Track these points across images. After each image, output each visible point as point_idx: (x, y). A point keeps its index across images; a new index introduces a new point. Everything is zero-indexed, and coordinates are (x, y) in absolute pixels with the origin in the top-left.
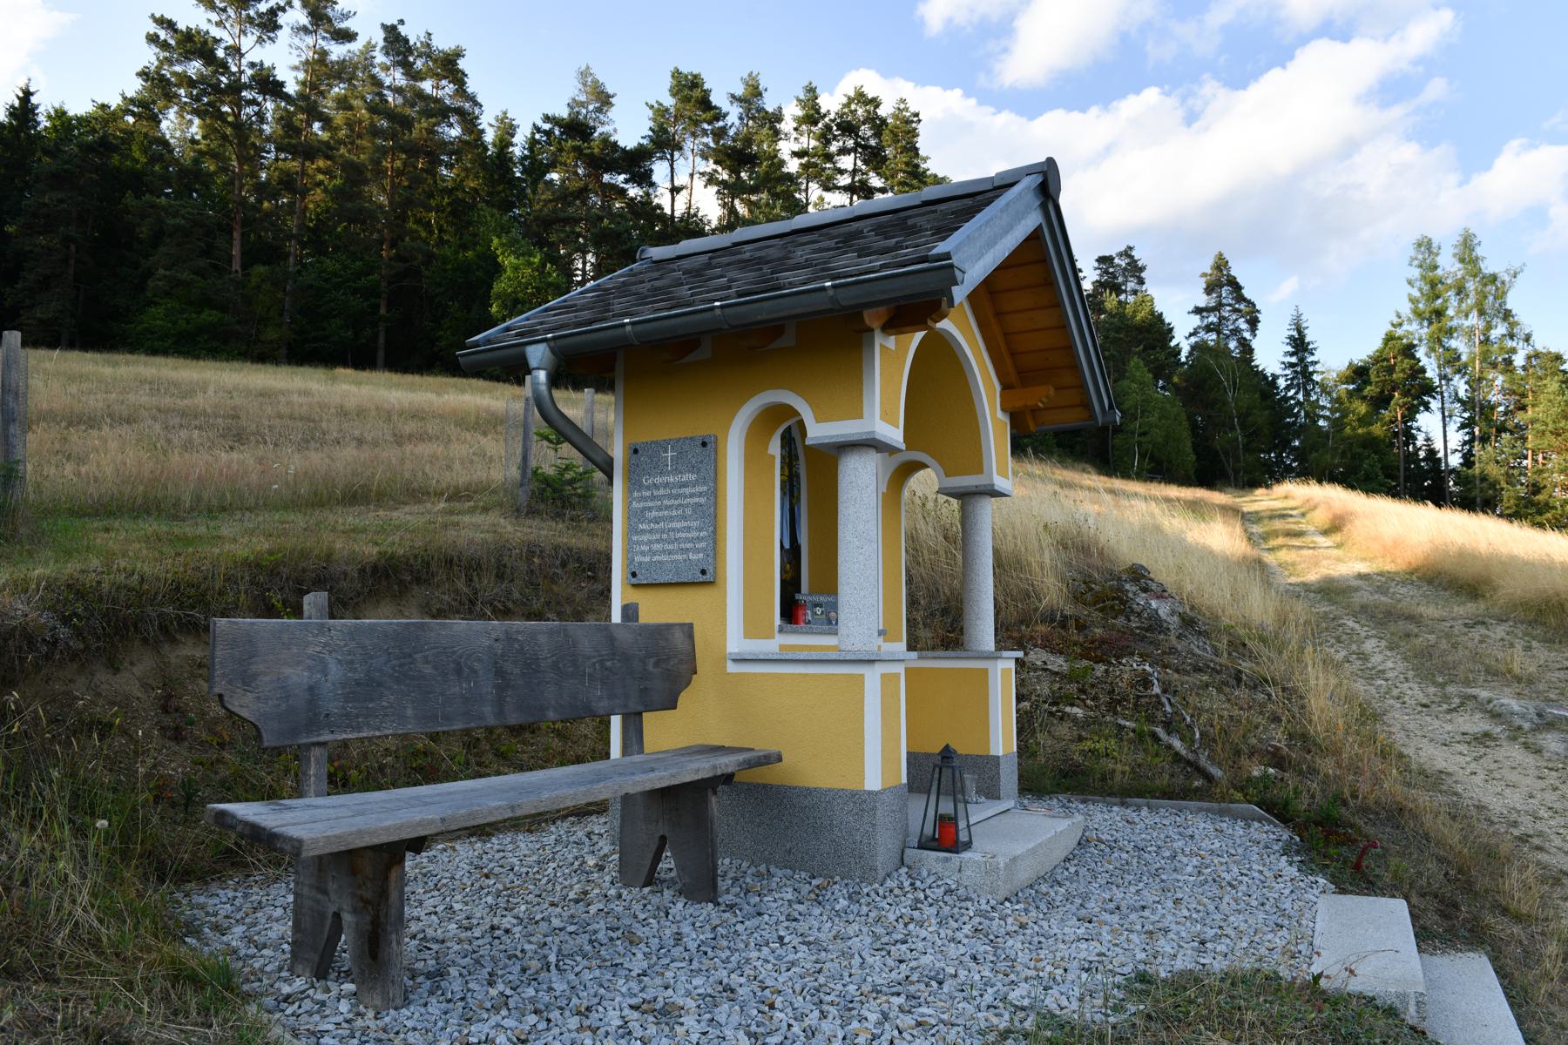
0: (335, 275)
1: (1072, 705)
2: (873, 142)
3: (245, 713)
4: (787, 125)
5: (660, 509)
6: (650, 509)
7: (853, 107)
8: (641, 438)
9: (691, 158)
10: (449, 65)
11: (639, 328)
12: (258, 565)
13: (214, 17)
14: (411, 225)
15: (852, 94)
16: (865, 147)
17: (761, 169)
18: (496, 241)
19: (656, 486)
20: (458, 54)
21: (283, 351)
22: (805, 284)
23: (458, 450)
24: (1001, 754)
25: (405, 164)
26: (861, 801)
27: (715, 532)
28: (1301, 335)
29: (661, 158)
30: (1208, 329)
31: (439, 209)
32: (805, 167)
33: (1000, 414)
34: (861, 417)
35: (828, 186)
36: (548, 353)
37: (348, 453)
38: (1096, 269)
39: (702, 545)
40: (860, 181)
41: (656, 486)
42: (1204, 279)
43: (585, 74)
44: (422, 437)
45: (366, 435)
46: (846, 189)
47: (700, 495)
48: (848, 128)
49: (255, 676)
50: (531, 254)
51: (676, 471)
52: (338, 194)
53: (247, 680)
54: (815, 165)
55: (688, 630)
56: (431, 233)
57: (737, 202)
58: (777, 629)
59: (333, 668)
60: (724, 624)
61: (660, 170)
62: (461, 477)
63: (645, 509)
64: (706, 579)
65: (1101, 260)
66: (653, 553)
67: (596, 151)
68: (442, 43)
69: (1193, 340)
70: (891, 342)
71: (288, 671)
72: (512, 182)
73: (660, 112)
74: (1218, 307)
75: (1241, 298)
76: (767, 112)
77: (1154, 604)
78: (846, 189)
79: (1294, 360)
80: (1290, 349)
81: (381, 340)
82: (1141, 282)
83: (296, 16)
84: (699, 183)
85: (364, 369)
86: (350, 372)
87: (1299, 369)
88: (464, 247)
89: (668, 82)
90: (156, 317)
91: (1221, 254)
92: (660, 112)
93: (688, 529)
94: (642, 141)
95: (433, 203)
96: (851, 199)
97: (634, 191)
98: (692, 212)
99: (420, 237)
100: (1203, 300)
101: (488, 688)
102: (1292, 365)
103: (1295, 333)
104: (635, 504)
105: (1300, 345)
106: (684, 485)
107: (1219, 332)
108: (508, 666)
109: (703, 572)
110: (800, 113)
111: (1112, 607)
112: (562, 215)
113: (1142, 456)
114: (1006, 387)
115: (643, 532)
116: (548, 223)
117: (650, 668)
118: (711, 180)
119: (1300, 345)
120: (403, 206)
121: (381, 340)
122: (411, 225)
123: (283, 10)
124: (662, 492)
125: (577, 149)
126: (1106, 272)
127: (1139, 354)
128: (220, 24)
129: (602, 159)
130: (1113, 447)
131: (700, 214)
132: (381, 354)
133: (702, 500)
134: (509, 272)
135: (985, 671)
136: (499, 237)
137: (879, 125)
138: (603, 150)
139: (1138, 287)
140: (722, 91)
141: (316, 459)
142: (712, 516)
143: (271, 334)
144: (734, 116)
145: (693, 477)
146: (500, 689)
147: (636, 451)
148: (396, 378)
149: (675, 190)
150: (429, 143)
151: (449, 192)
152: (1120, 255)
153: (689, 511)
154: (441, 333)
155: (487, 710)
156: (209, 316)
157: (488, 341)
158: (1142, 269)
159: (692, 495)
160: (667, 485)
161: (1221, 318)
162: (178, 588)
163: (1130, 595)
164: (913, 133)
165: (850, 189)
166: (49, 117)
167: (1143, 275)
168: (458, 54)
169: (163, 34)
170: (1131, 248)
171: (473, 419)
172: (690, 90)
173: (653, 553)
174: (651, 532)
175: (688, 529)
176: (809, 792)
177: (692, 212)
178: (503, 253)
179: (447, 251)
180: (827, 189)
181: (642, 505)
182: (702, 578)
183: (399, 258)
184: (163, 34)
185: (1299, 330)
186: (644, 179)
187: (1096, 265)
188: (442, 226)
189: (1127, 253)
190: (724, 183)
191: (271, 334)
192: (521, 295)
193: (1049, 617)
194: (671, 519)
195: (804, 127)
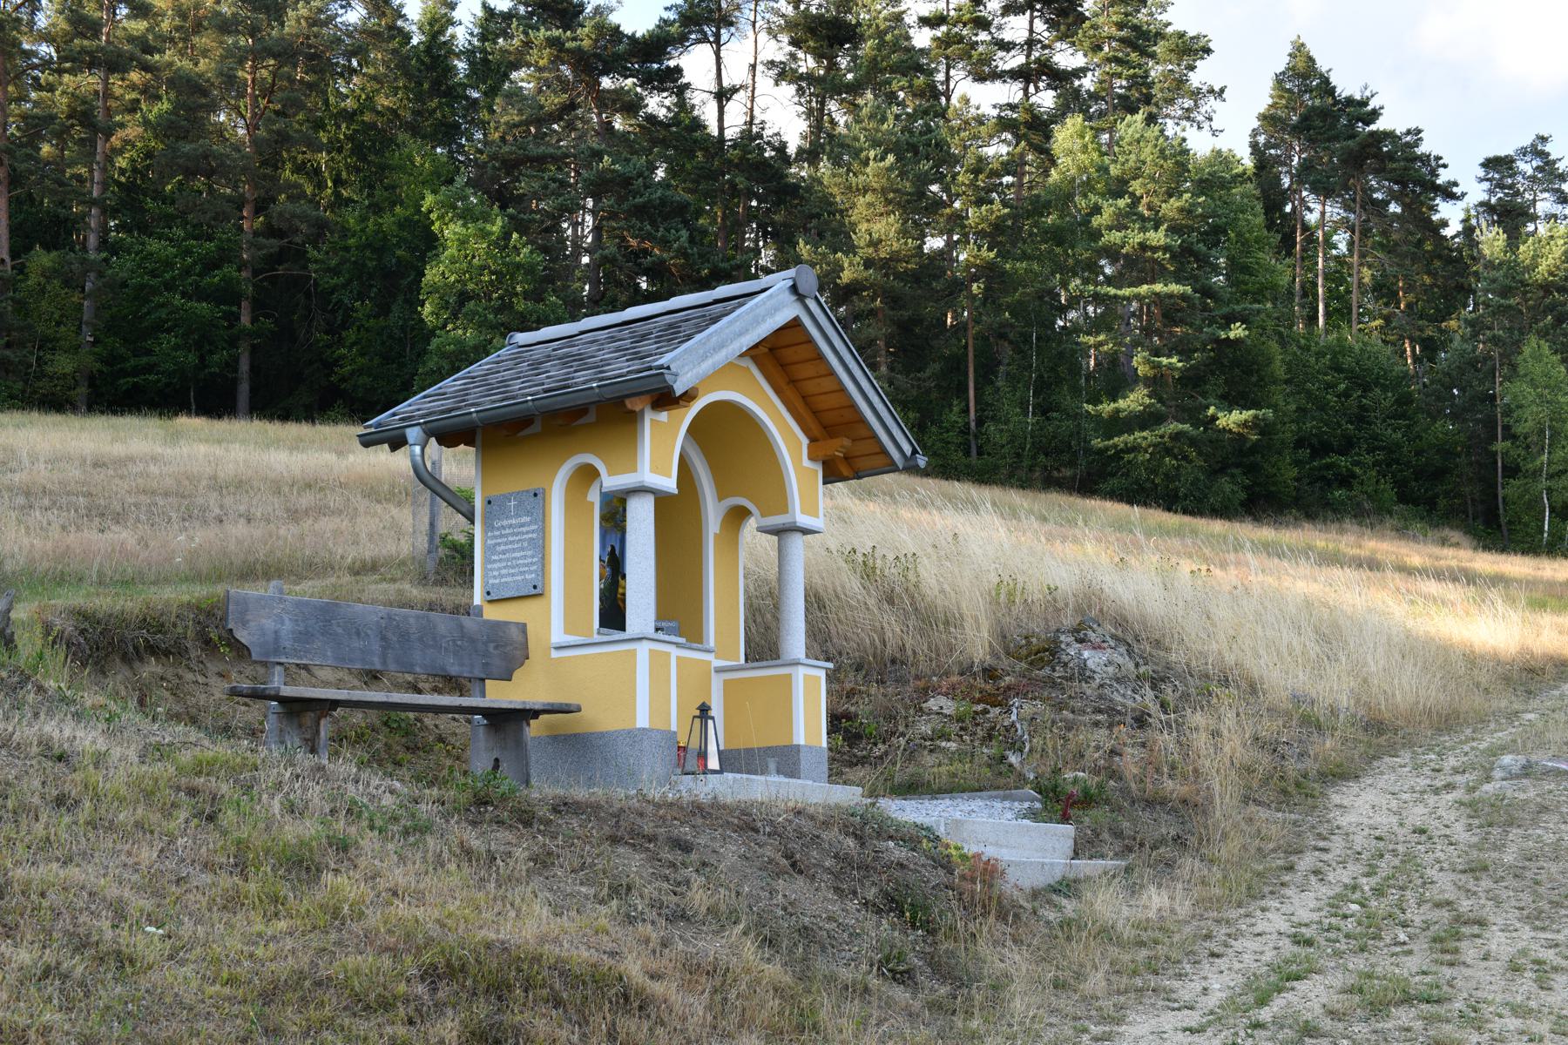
0: (169, 264)
1: (949, 740)
3: (243, 641)
5: (506, 544)
6: (499, 544)
8: (494, 493)
9: (751, 34)
11: (482, 414)
12: (198, 608)
14: (287, 174)
17: (867, 47)
18: (429, 200)
19: (503, 527)
21: (83, 390)
22: (584, 384)
23: (365, 525)
24: (802, 742)
25: (274, 74)
26: (636, 736)
27: (543, 558)
29: (698, 41)
31: (334, 147)
32: (944, 43)
33: (806, 463)
34: (635, 471)
35: (984, 73)
36: (421, 433)
37: (239, 530)
38: (1481, 180)
39: (535, 567)
40: (1038, 61)
41: (503, 527)
44: (322, 511)
45: (253, 510)
46: (1015, 74)
47: (533, 531)
49: (248, 621)
50: (486, 218)
51: (517, 516)
52: (167, 129)
53: (244, 623)
54: (960, 39)
55: (523, 628)
56: (321, 186)
57: (832, 106)
58: (595, 631)
59: (287, 622)
60: (549, 624)
61: (695, 64)
62: (368, 551)
63: (496, 544)
64: (536, 593)
65: (1491, 164)
66: (502, 576)
67: (586, 43)
70: (663, 416)
71: (264, 621)
72: (452, 94)
77: (1086, 654)
78: (1015, 74)
81: (244, 366)
84: (765, 82)
85: (220, 417)
86: (198, 422)
88: (376, 209)
93: (525, 557)
94: (666, 15)
95: (323, 137)
96: (1026, 90)
97: (657, 104)
98: (755, 129)
99: (303, 195)
101: (376, 646)
104: (489, 542)
106: (522, 525)
108: (389, 635)
109: (535, 587)
111: (1042, 659)
112: (535, 150)
114: (813, 440)
115: (495, 561)
116: (511, 166)
117: (491, 650)
118: (784, 73)
120: (271, 151)
121: (244, 366)
122: (287, 174)
124: (507, 531)
125: (553, 42)
126: (1501, 186)
127: (1543, 334)
129: (595, 55)
130: (1504, 498)
131: (767, 133)
132: (244, 389)
133: (534, 535)
134: (451, 251)
135: (790, 675)
136: (434, 192)
138: (596, 41)
141: (201, 537)
142: (541, 547)
143: (63, 364)
145: (528, 519)
146: (384, 648)
147: (489, 502)
148: (274, 429)
149: (723, 95)
150: (312, 41)
151: (349, 116)
152: (1523, 152)
153: (525, 544)
154: (343, 351)
155: (376, 660)
157: (379, 425)
159: (527, 532)
160: (510, 526)
162: (145, 620)
163: (1063, 646)
165: (1023, 75)
170: (1544, 139)
171: (386, 487)
173: (502, 576)
174: (500, 561)
175: (525, 557)
176: (602, 735)
177: (755, 129)
178: (441, 217)
179: (351, 219)
180: (980, 78)
181: (493, 542)
182: (534, 592)
183: (270, 231)
186: (670, 80)
187: (1481, 173)
188: (339, 175)
189: (1537, 150)
190: (810, 77)
191: (63, 364)
192: (471, 286)
194: (514, 550)
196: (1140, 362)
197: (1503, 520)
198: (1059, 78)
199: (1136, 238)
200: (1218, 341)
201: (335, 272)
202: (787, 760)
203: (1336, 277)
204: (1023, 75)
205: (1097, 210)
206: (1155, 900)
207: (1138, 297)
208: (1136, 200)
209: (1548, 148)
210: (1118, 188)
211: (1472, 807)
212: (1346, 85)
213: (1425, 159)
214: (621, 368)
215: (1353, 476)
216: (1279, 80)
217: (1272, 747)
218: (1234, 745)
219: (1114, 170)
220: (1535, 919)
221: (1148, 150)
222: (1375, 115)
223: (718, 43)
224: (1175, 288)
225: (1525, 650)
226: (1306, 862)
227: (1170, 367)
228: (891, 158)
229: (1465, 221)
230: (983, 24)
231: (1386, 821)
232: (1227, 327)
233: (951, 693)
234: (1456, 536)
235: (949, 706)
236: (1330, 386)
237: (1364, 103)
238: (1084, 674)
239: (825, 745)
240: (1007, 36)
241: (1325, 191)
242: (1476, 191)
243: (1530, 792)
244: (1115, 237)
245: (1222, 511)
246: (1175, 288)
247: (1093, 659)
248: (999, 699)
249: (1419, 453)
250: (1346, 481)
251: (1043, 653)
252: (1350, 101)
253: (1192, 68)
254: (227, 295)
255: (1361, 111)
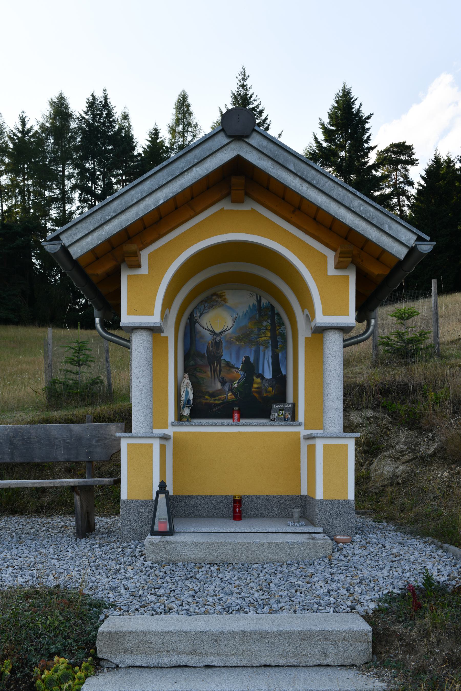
239: (351, 496)
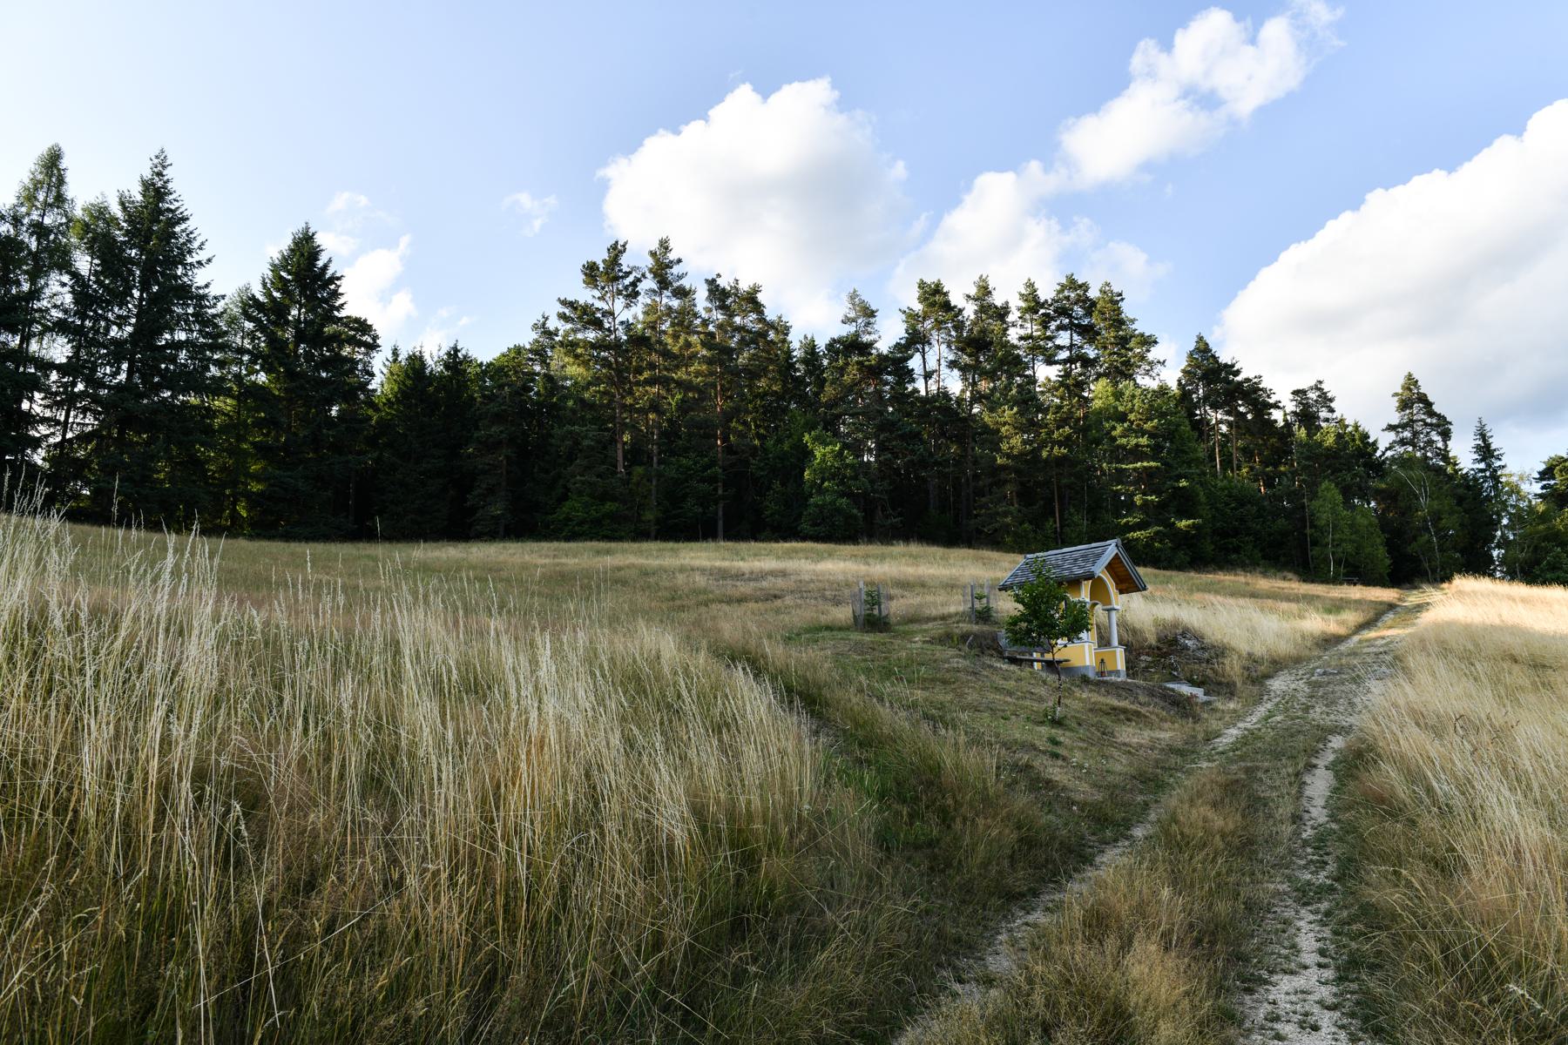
2: (1085, 322)
4: (1013, 317)
7: (1066, 293)
10: (751, 301)
13: (597, 293)
15: (1064, 281)
16: (1079, 326)
18: (806, 437)
20: (755, 290)
28: (1488, 446)
30: (1403, 442)
35: (1050, 361)
42: (1396, 398)
43: (853, 296)
48: (1063, 312)
54: (1040, 347)
65: (1296, 393)
68: (744, 286)
69: (1389, 454)
73: (911, 317)
74: (1409, 424)
75: (1432, 414)
76: (996, 307)
79: (1482, 466)
80: (1476, 456)
81: (720, 513)
82: (1332, 411)
83: (649, 283)
84: (945, 371)
87: (1488, 474)
89: (915, 293)
90: (573, 507)
91: (1410, 375)
92: (911, 317)
100: (1395, 419)
102: (1481, 471)
103: (1480, 442)
105: (1486, 452)
107: (1414, 446)
110: (1023, 304)
113: (1338, 563)
118: (953, 364)
119: (1486, 452)
123: (639, 280)
128: (602, 298)
137: (1090, 306)
139: (1329, 415)
140: (959, 294)
144: (970, 311)
156: (610, 506)
158: (1331, 400)
161: (1415, 434)
164: (1118, 311)
166: (84, 210)
167: (1332, 405)
168: (755, 290)
169: (567, 311)
170: (1320, 382)
172: (934, 296)
184: (567, 311)
185: (1483, 436)
187: (1291, 397)
189: (1317, 387)
193: (1150, 647)
195: (1027, 316)
196: (1138, 499)
197: (1312, 566)
198: (1087, 362)
199: (1134, 441)
200: (1174, 488)
201: (762, 469)
202: (1117, 673)
203: (1223, 446)
204: (1070, 360)
205: (1114, 428)
206: (1232, 705)
207: (1135, 469)
208: (1132, 423)
209: (1323, 386)
210: (1122, 418)
211: (1309, 683)
212: (1224, 359)
213: (1264, 390)
214: (1078, 571)
215: (1239, 547)
216: (1191, 354)
217: (1248, 669)
218: (1237, 668)
219: (1121, 409)
220: (1327, 706)
221: (1135, 401)
222: (1238, 373)
223: (923, 354)
224: (1153, 464)
225: (1324, 633)
226: (1265, 698)
227: (1152, 501)
228: (1015, 409)
229: (1285, 420)
230: (1050, 338)
231: (1285, 688)
232: (1178, 481)
233: (1148, 654)
234: (1290, 575)
235: (1149, 659)
236: (1227, 504)
237: (1233, 366)
238: (1186, 648)
240: (1058, 342)
241: (1215, 407)
242: (1291, 407)
243: (1326, 679)
244: (1124, 441)
245: (1180, 568)
246: (1153, 464)
247: (1189, 643)
248: (1165, 655)
249: (1270, 535)
250: (1237, 550)
251: (1174, 641)
252: (1226, 365)
253: (1148, 351)
254: (713, 480)
255: (1230, 369)
